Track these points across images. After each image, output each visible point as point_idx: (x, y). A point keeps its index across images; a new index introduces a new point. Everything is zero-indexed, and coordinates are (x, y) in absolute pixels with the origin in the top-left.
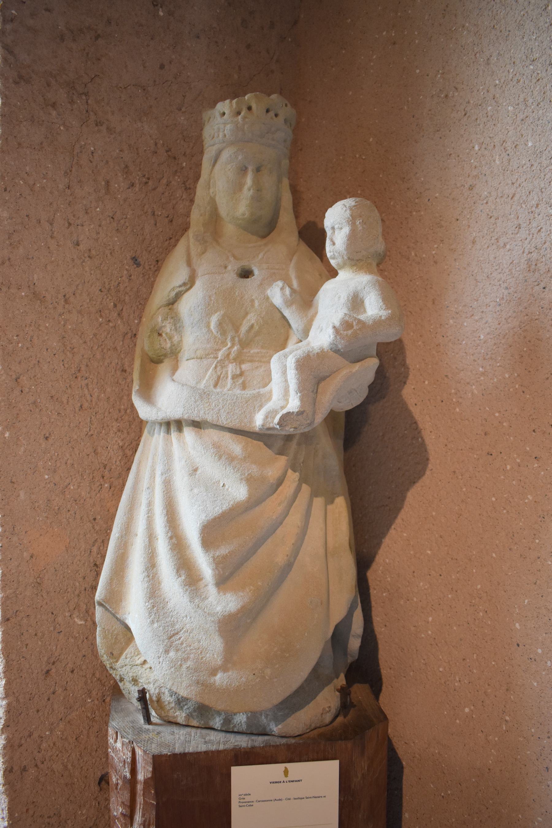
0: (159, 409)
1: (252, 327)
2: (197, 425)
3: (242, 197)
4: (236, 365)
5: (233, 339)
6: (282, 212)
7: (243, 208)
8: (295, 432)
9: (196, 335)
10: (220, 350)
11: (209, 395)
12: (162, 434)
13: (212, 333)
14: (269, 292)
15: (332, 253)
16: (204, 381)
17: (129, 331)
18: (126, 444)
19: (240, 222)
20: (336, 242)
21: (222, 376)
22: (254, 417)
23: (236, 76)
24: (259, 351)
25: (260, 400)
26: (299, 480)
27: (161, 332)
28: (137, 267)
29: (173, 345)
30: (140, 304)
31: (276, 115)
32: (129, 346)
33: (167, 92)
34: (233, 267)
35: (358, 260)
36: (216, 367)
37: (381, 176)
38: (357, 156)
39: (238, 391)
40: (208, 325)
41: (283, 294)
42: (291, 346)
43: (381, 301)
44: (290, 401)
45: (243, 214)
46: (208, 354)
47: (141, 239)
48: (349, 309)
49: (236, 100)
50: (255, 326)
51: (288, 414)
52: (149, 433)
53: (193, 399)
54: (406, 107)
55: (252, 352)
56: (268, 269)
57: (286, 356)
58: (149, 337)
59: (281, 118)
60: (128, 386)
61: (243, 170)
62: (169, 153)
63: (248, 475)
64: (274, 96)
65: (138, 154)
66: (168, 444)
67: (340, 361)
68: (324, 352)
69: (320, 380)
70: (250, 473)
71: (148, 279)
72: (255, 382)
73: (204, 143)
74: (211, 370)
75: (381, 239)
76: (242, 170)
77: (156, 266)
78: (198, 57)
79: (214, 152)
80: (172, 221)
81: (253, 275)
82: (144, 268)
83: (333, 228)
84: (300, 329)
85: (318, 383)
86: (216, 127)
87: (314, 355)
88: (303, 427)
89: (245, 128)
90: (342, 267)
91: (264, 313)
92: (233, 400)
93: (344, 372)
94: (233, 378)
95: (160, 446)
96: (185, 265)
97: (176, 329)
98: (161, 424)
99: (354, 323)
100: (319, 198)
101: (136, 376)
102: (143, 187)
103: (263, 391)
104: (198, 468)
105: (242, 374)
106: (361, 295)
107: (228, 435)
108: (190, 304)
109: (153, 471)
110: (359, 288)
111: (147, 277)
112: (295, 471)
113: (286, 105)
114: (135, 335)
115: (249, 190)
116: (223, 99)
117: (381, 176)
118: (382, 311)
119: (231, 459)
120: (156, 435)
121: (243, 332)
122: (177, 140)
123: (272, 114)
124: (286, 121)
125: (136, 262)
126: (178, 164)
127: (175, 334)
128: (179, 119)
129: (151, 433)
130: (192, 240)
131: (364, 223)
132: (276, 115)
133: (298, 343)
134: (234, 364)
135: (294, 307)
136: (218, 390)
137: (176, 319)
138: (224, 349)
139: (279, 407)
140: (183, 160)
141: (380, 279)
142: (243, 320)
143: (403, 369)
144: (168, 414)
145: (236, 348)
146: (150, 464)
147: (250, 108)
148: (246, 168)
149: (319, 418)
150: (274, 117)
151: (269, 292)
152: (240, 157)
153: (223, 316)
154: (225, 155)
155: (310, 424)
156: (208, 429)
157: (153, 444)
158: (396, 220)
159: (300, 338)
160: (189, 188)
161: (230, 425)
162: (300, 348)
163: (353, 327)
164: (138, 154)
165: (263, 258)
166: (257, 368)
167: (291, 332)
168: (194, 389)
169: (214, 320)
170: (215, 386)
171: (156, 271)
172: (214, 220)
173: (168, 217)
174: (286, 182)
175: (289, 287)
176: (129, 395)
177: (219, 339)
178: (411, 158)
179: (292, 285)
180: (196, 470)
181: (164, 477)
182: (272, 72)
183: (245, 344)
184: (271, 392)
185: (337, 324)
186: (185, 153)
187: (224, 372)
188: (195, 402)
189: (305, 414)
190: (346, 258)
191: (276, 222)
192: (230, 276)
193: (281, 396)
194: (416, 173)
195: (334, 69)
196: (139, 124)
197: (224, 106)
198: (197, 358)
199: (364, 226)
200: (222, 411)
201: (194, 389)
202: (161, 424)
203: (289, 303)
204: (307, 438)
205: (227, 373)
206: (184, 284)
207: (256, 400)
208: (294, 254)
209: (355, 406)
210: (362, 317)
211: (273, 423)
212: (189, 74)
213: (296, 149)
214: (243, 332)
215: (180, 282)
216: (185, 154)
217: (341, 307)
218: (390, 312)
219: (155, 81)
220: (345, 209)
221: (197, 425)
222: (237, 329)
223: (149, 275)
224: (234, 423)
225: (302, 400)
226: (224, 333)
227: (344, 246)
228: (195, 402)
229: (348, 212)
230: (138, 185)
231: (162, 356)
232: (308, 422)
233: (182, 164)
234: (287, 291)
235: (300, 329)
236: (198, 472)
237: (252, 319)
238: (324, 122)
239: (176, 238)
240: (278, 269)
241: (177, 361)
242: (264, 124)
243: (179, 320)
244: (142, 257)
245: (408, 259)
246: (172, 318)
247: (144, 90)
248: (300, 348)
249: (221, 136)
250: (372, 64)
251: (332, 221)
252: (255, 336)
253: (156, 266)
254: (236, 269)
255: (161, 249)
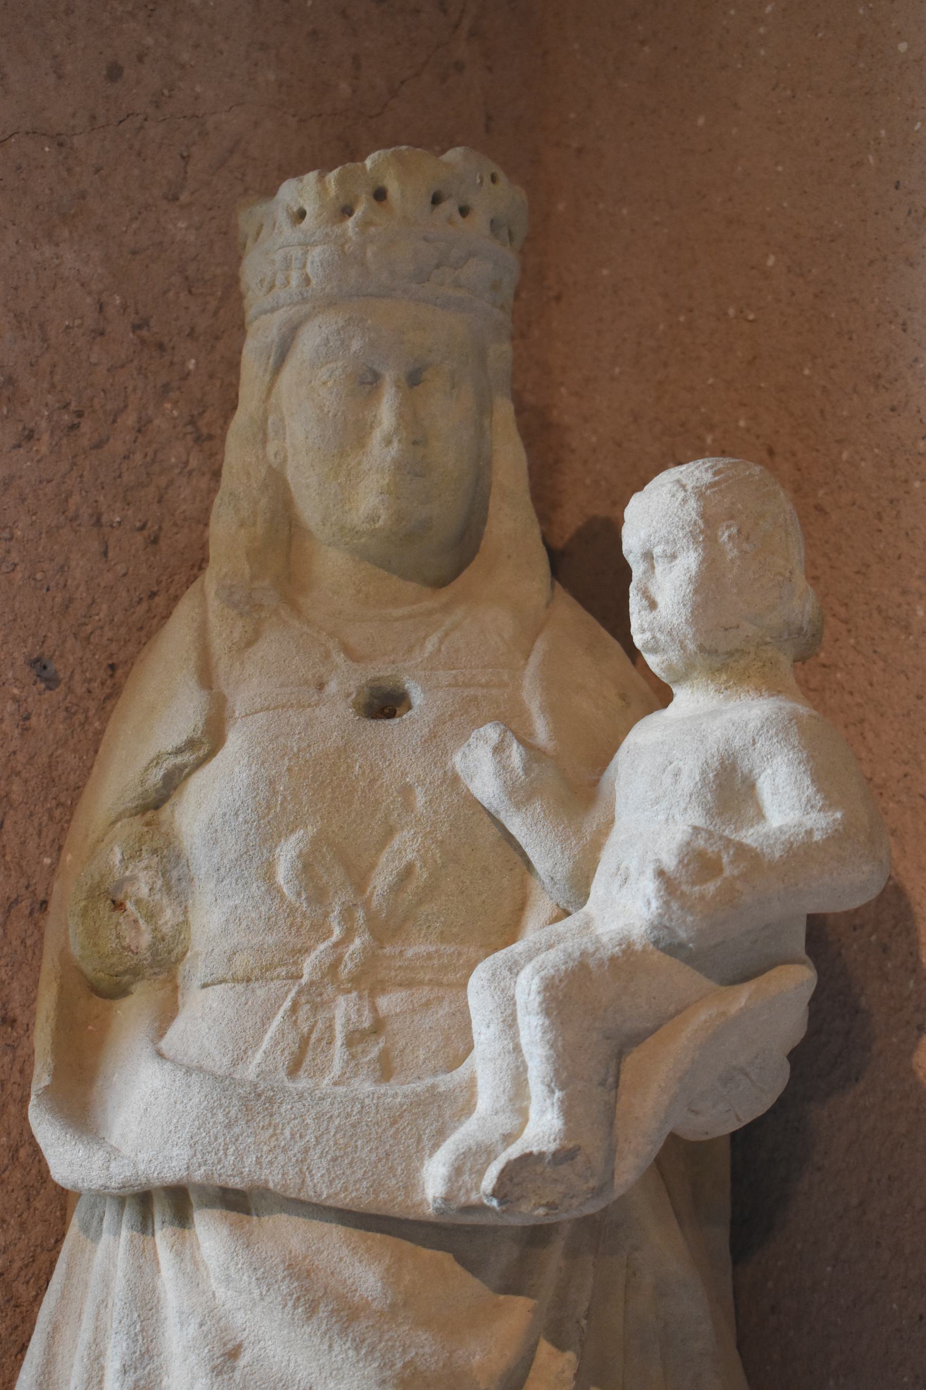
0: (113, 1153)
1: (408, 872)
2: (236, 1202)
3: (365, 466)
4: (360, 997)
5: (347, 915)
6: (494, 503)
7: (369, 500)
8: (553, 1219)
9: (231, 903)
10: (307, 950)
11: (271, 1100)
12: (125, 1233)
13: (283, 896)
14: (458, 761)
15: (648, 635)
16: (259, 1056)
17: (23, 891)
18: (17, 1265)
19: (363, 540)
20: (659, 599)
21: (314, 1037)
22: (418, 1170)
23: (344, 88)
24: (432, 949)
25: (441, 1111)
26: (576, 1376)
27: (120, 897)
28: (49, 688)
29: (159, 938)
30: (59, 804)
31: (464, 211)
32: (23, 942)
33: (131, 147)
34: (345, 682)
35: (730, 654)
36: (294, 1009)
37: (807, 372)
38: (731, 312)
39: (365, 1087)
40: (269, 875)
41: (503, 767)
42: (533, 932)
43: (807, 781)
44: (533, 1114)
45: (373, 519)
46: (270, 967)
47: (58, 600)
48: (708, 812)
49: (335, 172)
50: (417, 869)
51: (526, 1159)
52: (85, 1228)
53: (220, 1117)
54: (871, 158)
55: (410, 953)
56: (456, 685)
57: (514, 968)
58: (84, 913)
59: (480, 220)
60: (21, 1071)
61: (367, 383)
62: (144, 333)
63: (405, 1366)
64: (454, 155)
65: (44, 340)
66: (144, 1264)
67: (687, 979)
68: (634, 953)
69: (624, 1044)
70: (411, 1362)
71: (82, 725)
72: (421, 1054)
73: (246, 302)
74: (278, 1019)
75: (801, 581)
76: (362, 383)
77: (109, 683)
78: (227, 38)
79: (275, 331)
80: (155, 541)
81: (410, 707)
82: (70, 690)
83: (648, 556)
84: (558, 877)
85: (620, 1055)
86: (278, 257)
87: (601, 965)
88: (575, 1202)
89: (369, 254)
90: (685, 675)
91: (445, 828)
92: (349, 1115)
93: (703, 1016)
94: (350, 1042)
95: (120, 1274)
96: (193, 683)
97: (168, 888)
98: (121, 1201)
99: (725, 859)
100: (619, 445)
101: (42, 1039)
102: (65, 441)
103: (445, 1081)
104: (240, 1346)
105: (378, 1027)
106: (744, 765)
107: (336, 1233)
108: (208, 808)
109: (97, 1359)
110: (737, 743)
111: (81, 717)
112: (560, 1345)
113: (494, 179)
114: (44, 904)
115: (388, 442)
116: (298, 172)
117: (807, 372)
118: (814, 815)
119: (346, 1314)
120: (106, 1238)
121: (378, 890)
122: (165, 293)
123: (449, 207)
124: (494, 225)
125: (45, 674)
126: (172, 363)
127: (165, 901)
128: (170, 226)
129: (92, 1232)
130: (214, 604)
131: (742, 536)
132: (464, 211)
133: (556, 919)
134: (354, 994)
135: (537, 806)
136: (303, 1083)
137: (168, 857)
138: (322, 947)
139: (497, 1136)
140: (190, 351)
141: (803, 710)
142: (380, 851)
143: (911, 984)
144: (142, 1167)
145: (357, 943)
146: (85, 1335)
147: (380, 195)
148: (376, 377)
149: (629, 1169)
150: (457, 217)
151: (458, 761)
152: (356, 345)
153: (316, 841)
154: (309, 341)
155: (597, 1192)
156: (271, 1212)
157: (100, 1261)
158: (862, 508)
159: (563, 904)
160: (208, 441)
161: (344, 1200)
162: (560, 939)
163: (721, 870)
164: (44, 340)
165: (439, 650)
166: (427, 1004)
167: (534, 884)
168: (223, 1082)
169: (287, 855)
170: (294, 1069)
171: (108, 697)
172: (283, 536)
173: (142, 528)
174: (504, 409)
175: (521, 741)
176: (24, 1101)
177: (304, 915)
178: (896, 314)
179: (532, 734)
180: (234, 1354)
181: (131, 1378)
182: (459, 67)
183: (387, 929)
184: (471, 1084)
185: (670, 863)
186: (193, 329)
187: (320, 1025)
188: (229, 1126)
189: (580, 1159)
190: (691, 647)
191: (480, 536)
192: (336, 713)
193: (503, 1099)
194: (916, 360)
195: (647, 49)
196: (48, 251)
197: (301, 191)
198: (235, 980)
199: (746, 546)
200: (314, 1155)
201: (223, 1082)
202: (121, 1201)
203: (521, 795)
204: (599, 1233)
205: (330, 1028)
206: (191, 744)
207: (425, 1114)
208: (537, 635)
209: (747, 1120)
210: (750, 836)
211: (478, 1189)
212: (198, 89)
213: (536, 298)
214: (378, 890)
215: (178, 740)
216: (192, 334)
217: (683, 805)
218: (838, 815)
219: (93, 118)
220: (681, 495)
221: (236, 1202)
222: (360, 881)
223: (86, 711)
224: (355, 1194)
225: (568, 1111)
226: (318, 895)
227: (685, 612)
228: (229, 1126)
229: (692, 503)
230: (46, 437)
231: (125, 972)
232: (593, 1183)
233: (183, 363)
234: (516, 755)
235: (558, 877)
236: (242, 1362)
237: (406, 846)
238: (625, 211)
239: (172, 591)
240: (486, 685)
241: (176, 988)
242: (426, 239)
243: (178, 857)
244: (61, 656)
245: (907, 629)
246: (155, 851)
247: (61, 145)
248: (560, 939)
249: (294, 283)
250: (762, 30)
251: (643, 534)
252: (420, 902)
253: (109, 683)
254: (352, 689)
255: (123, 630)
